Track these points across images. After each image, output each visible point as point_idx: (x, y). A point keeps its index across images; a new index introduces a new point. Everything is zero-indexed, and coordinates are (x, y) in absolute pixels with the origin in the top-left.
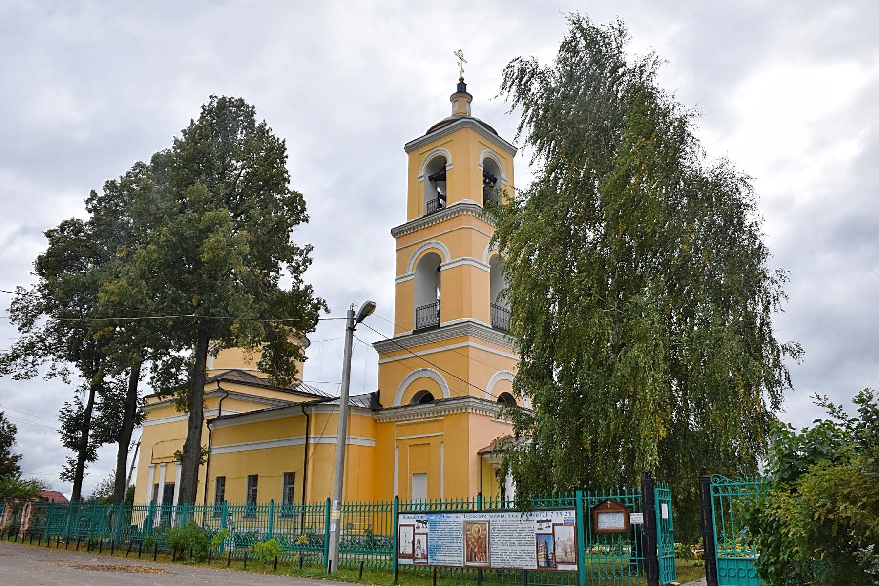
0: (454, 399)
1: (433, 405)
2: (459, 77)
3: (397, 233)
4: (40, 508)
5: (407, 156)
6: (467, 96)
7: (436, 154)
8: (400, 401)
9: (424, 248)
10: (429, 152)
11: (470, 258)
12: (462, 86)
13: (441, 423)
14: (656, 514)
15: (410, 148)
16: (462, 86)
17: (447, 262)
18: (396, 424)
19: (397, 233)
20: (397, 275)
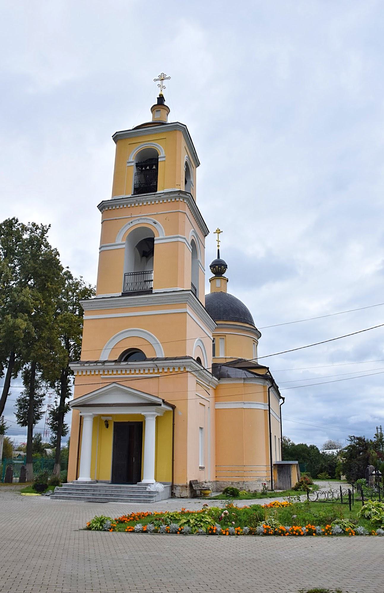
0: (166, 359)
1: (79, 365)
2: (159, 93)
3: (103, 206)
4: (57, 583)
5: (115, 145)
6: (165, 108)
7: (148, 146)
8: (107, 357)
9: (141, 221)
10: (143, 143)
11: (177, 235)
12: (161, 99)
13: (157, 380)
14: (289, 461)
15: (118, 137)
16: (161, 99)
17: (161, 237)
18: (102, 376)
19: (103, 206)
20: (101, 244)
